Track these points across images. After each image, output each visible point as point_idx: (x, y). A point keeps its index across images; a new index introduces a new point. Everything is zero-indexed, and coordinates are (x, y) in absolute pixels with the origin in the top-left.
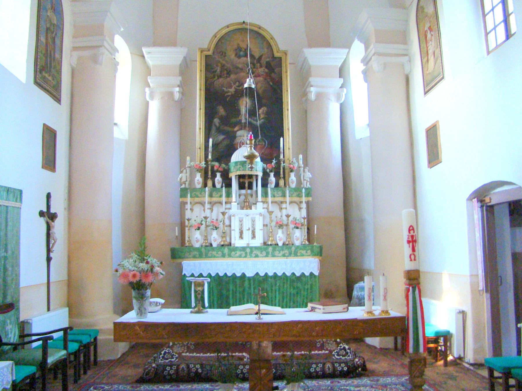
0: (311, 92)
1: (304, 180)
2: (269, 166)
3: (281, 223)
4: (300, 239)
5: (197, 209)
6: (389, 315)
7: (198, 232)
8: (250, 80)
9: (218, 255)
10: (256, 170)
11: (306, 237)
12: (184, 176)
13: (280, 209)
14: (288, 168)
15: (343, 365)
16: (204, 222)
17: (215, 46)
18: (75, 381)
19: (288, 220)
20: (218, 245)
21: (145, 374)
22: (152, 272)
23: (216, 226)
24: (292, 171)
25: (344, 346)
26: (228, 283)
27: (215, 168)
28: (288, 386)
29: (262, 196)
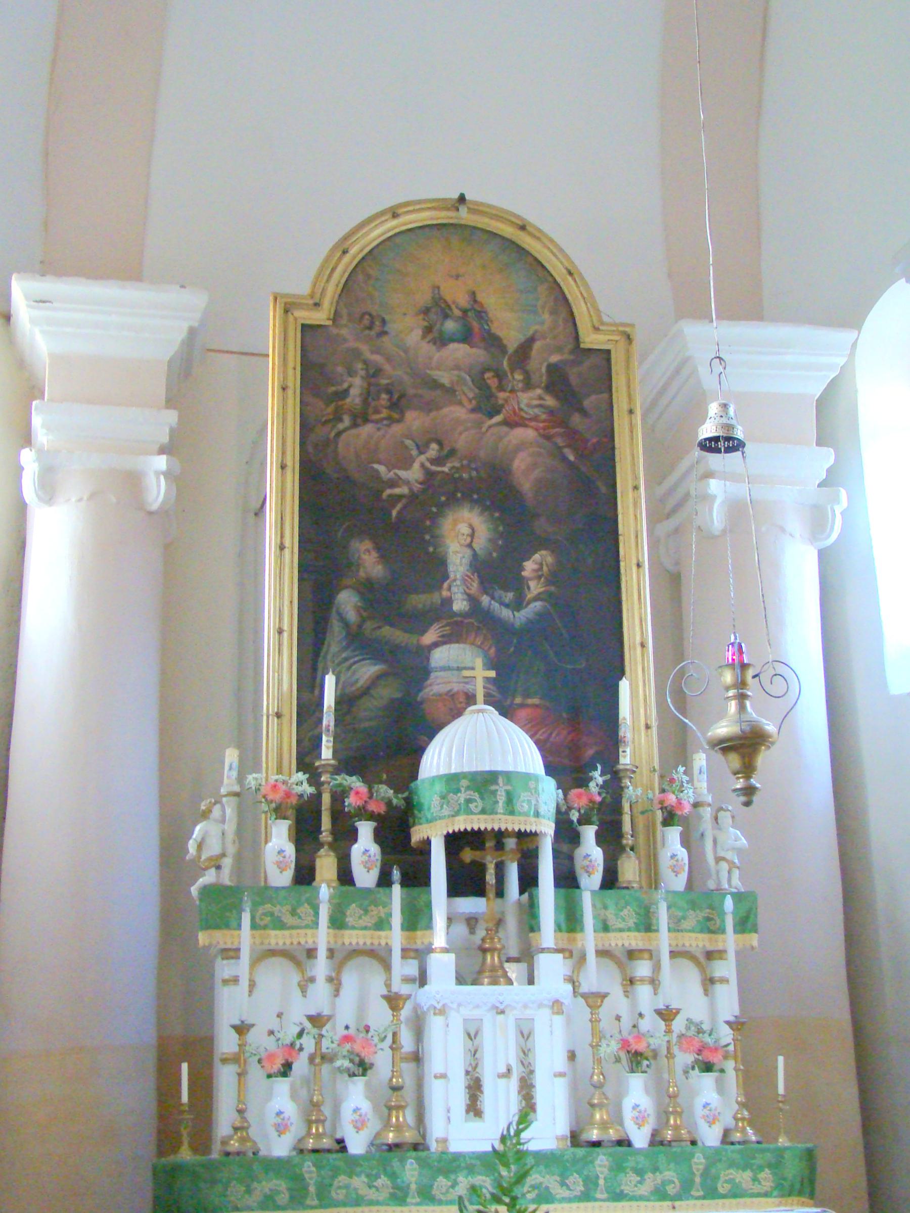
0: (708, 498)
1: (718, 859)
2: (579, 796)
7: (283, 1086)
16: (308, 1043)
19: (669, 1031)
27: (351, 802)
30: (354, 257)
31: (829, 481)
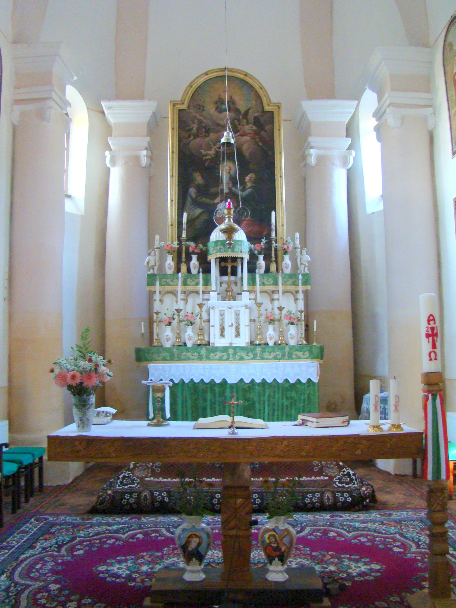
0: (310, 155)
1: (301, 264)
2: (258, 246)
3: (272, 318)
4: (295, 337)
5: (168, 299)
6: (400, 431)
7: (169, 328)
8: (228, 133)
9: (192, 357)
10: (241, 252)
11: (303, 335)
12: (152, 259)
13: (271, 301)
14: (282, 249)
15: (346, 495)
16: (176, 317)
17: (190, 98)
18: (14, 511)
19: (281, 313)
20: (193, 345)
21: (98, 503)
22: (96, 373)
23: (191, 320)
24: (286, 252)
25: (348, 471)
26: (205, 391)
27: (191, 250)
28: (272, 520)
29: (249, 284)
30: (194, 88)
31: (350, 148)
